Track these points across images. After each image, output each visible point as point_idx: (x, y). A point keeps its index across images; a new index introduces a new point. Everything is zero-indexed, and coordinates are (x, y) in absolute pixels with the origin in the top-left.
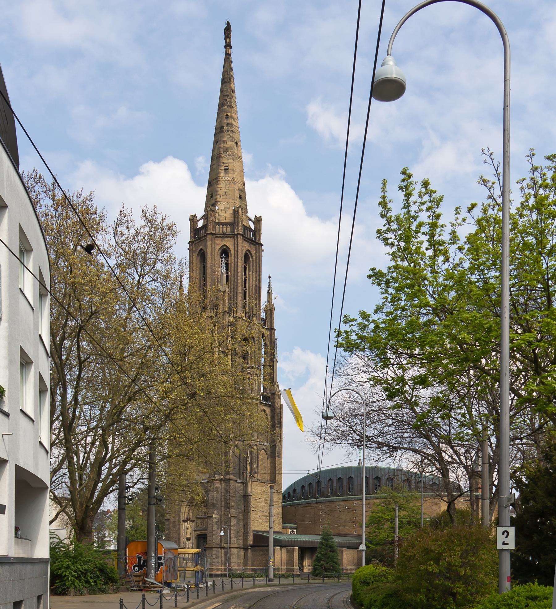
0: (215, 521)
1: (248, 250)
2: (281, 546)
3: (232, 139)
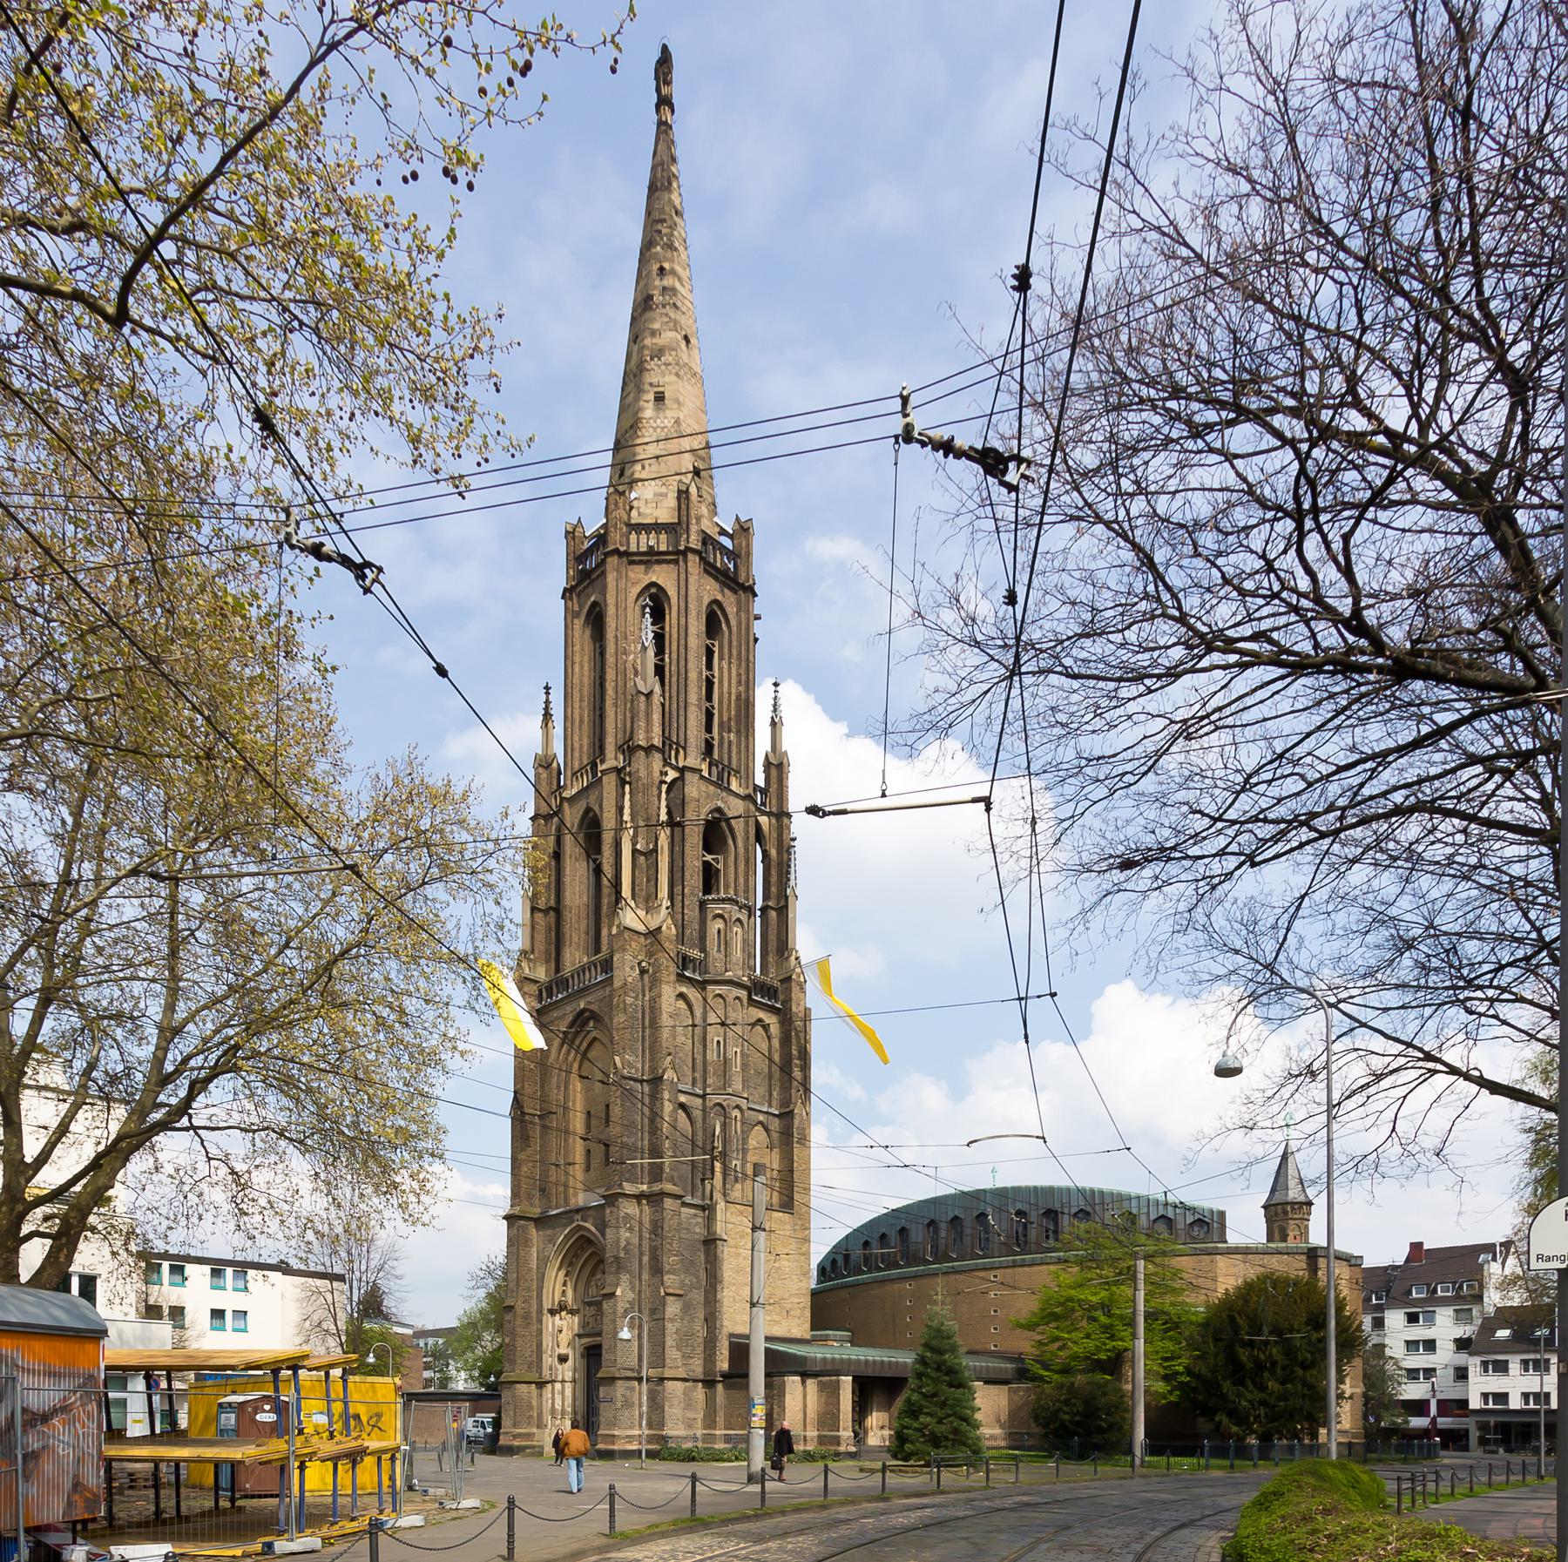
0: (621, 1306)
1: (716, 602)
2: (805, 1375)
3: (676, 326)
